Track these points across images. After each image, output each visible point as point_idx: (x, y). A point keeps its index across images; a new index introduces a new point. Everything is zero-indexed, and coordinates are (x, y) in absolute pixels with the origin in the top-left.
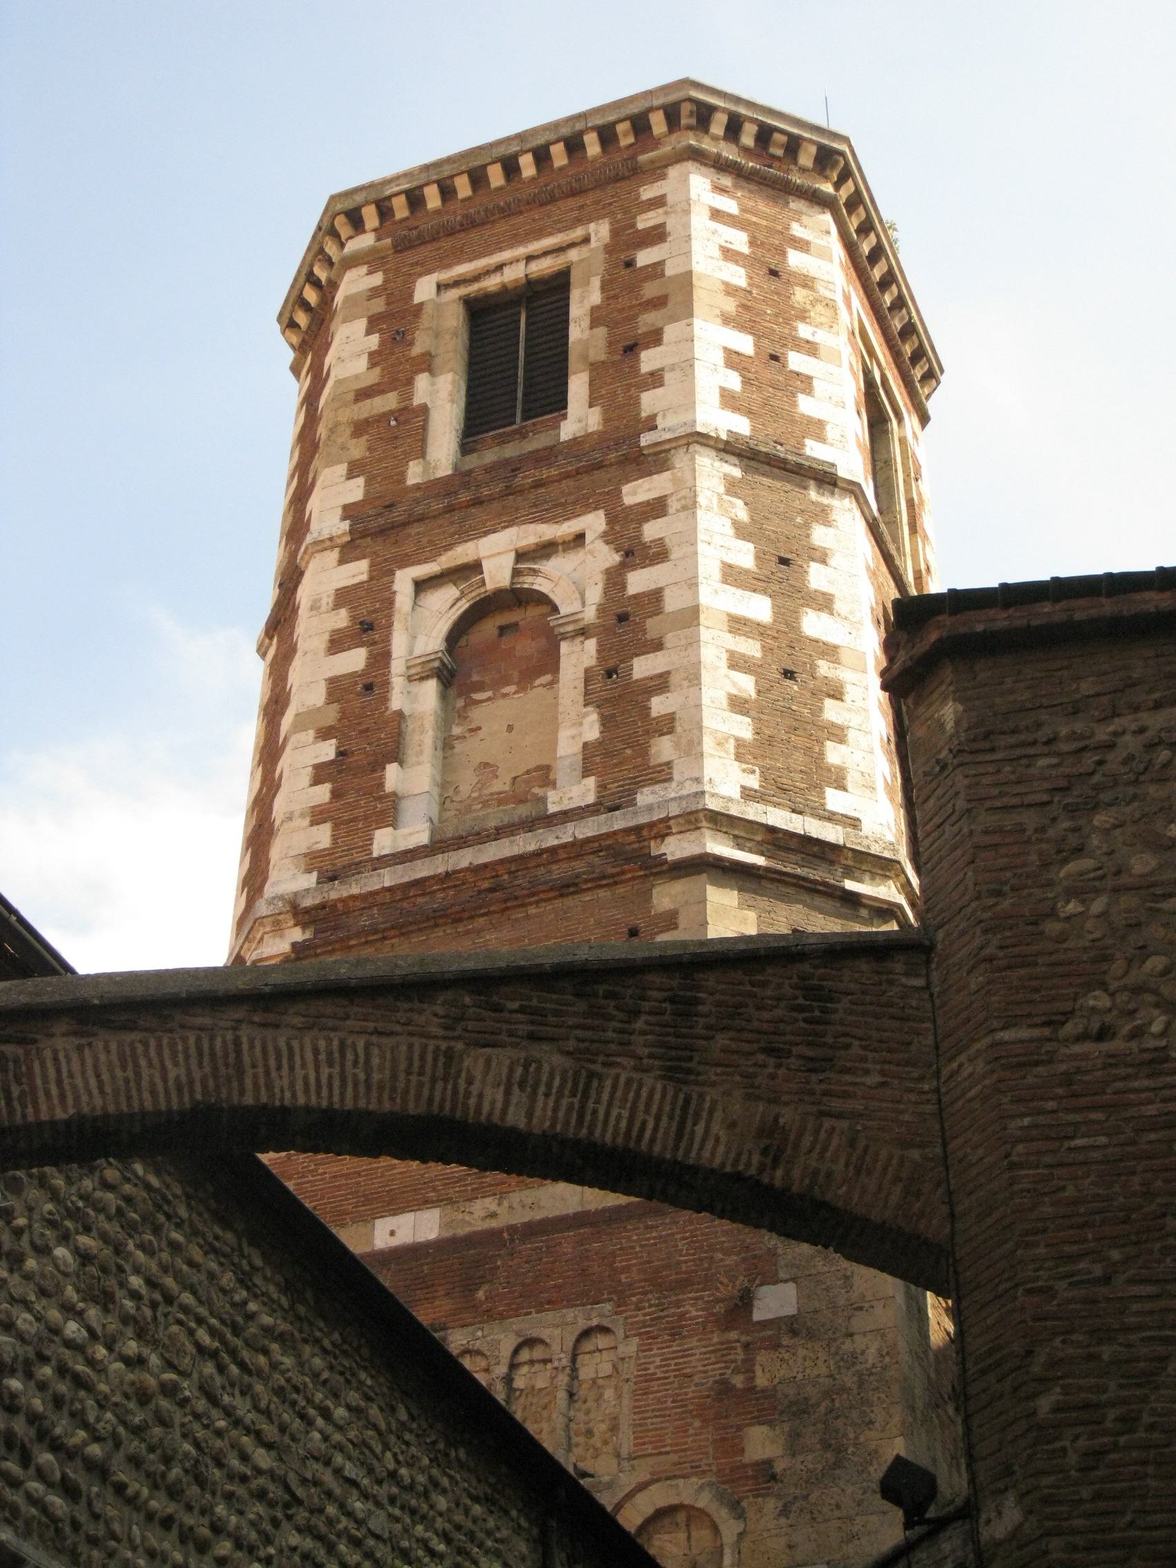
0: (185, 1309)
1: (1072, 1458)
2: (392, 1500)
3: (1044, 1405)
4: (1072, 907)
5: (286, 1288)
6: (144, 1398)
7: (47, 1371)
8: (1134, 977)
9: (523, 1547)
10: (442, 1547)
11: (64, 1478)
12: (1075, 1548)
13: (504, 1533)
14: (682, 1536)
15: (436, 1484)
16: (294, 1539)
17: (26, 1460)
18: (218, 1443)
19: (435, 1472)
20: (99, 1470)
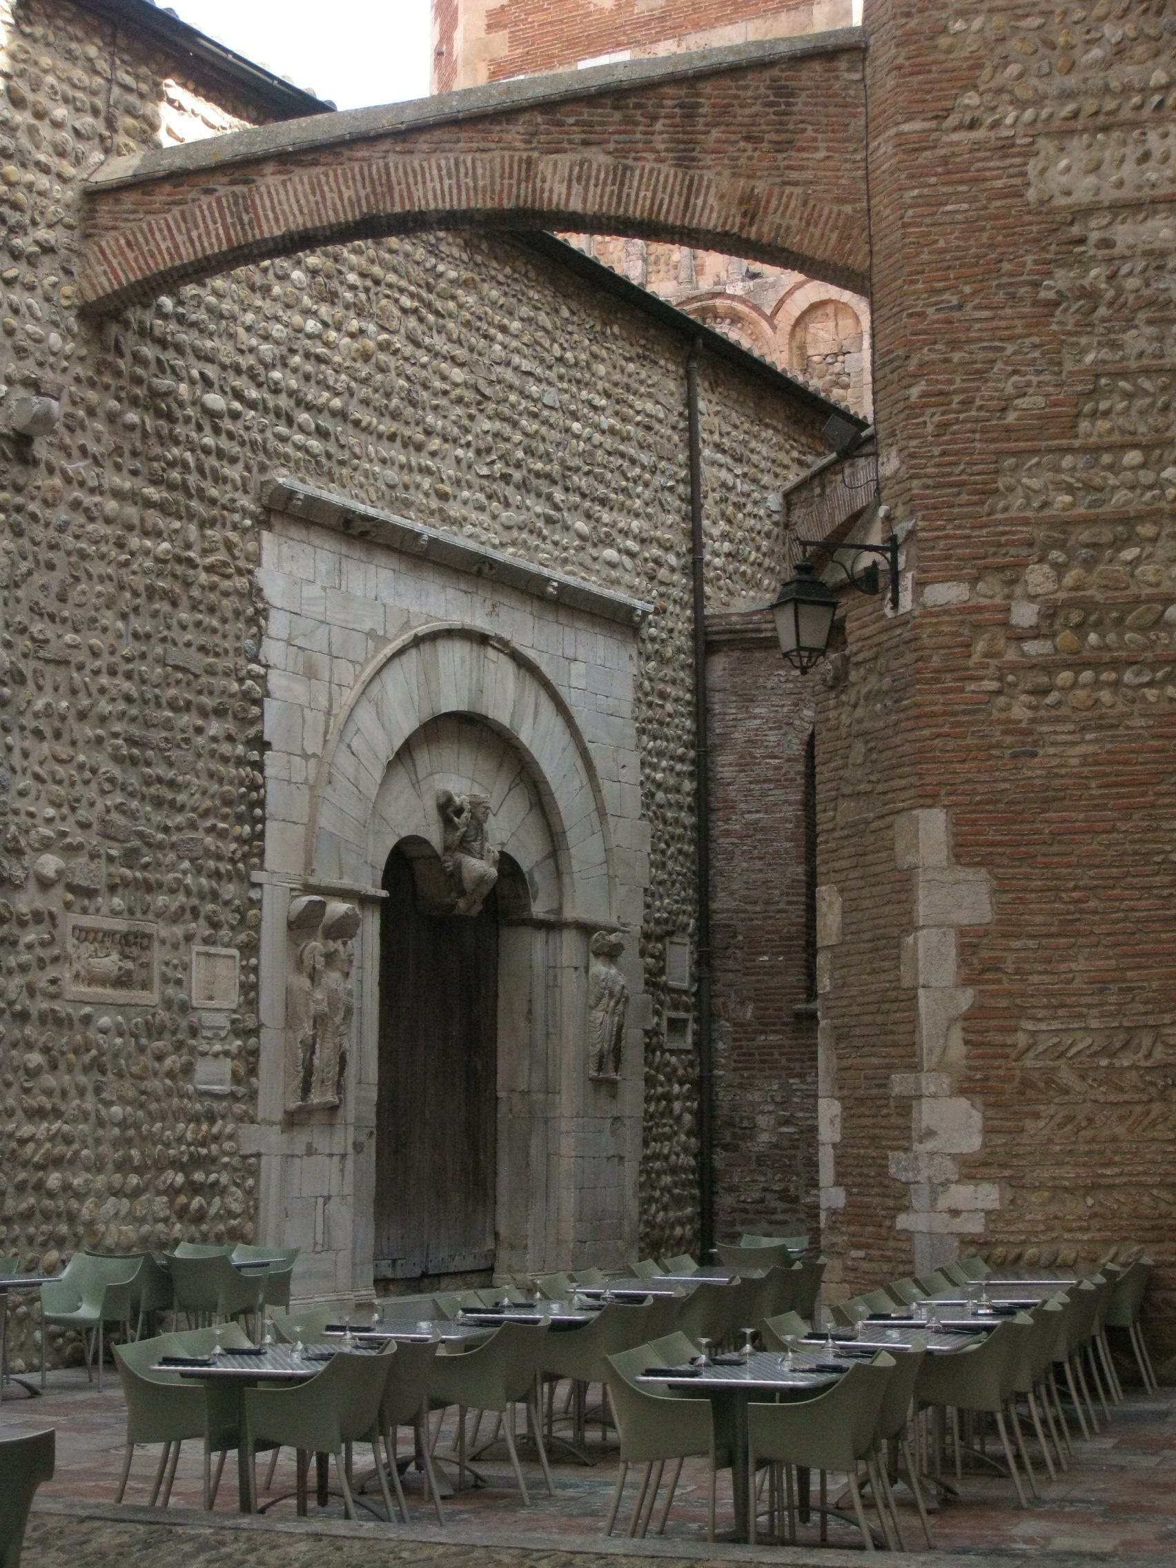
0: (390, 286)
1: (930, 428)
2: (561, 378)
3: (915, 392)
4: (959, 25)
5: (467, 246)
6: (366, 357)
7: (297, 359)
8: (998, 81)
9: (672, 385)
10: (604, 402)
11: (318, 427)
12: (927, 487)
13: (655, 378)
14: (831, 324)
15: (595, 356)
16: (487, 425)
17: (290, 422)
18: (424, 373)
19: (595, 348)
20: (342, 415)
